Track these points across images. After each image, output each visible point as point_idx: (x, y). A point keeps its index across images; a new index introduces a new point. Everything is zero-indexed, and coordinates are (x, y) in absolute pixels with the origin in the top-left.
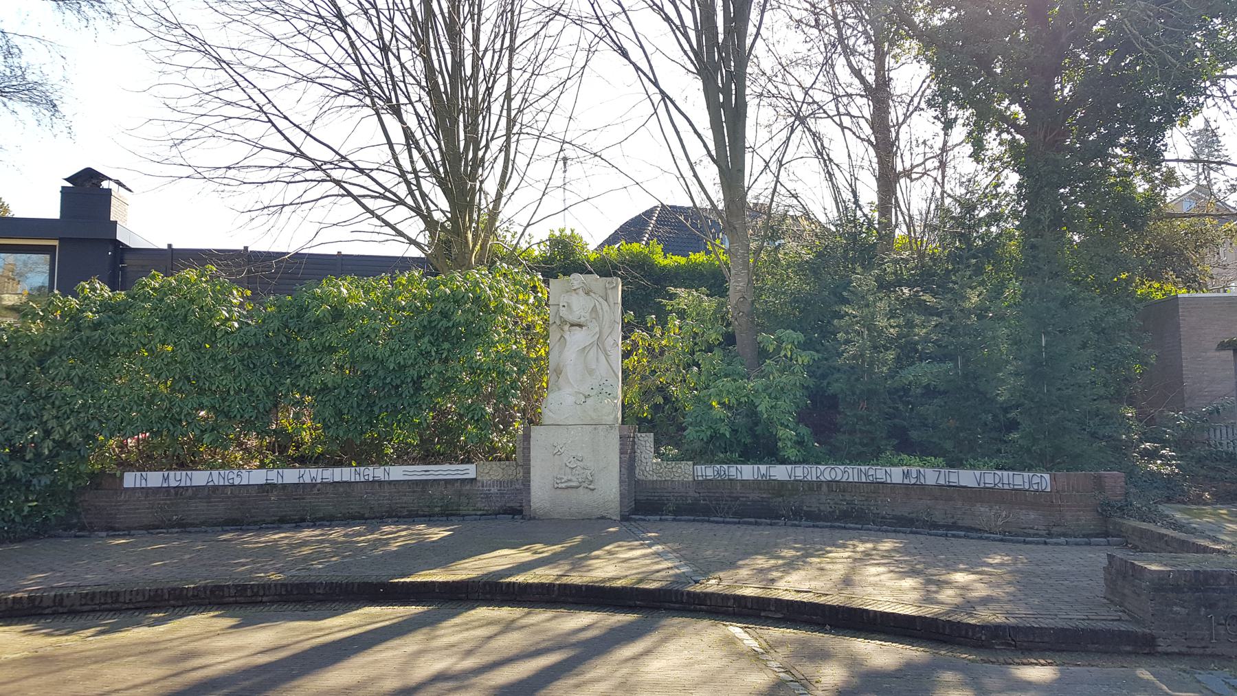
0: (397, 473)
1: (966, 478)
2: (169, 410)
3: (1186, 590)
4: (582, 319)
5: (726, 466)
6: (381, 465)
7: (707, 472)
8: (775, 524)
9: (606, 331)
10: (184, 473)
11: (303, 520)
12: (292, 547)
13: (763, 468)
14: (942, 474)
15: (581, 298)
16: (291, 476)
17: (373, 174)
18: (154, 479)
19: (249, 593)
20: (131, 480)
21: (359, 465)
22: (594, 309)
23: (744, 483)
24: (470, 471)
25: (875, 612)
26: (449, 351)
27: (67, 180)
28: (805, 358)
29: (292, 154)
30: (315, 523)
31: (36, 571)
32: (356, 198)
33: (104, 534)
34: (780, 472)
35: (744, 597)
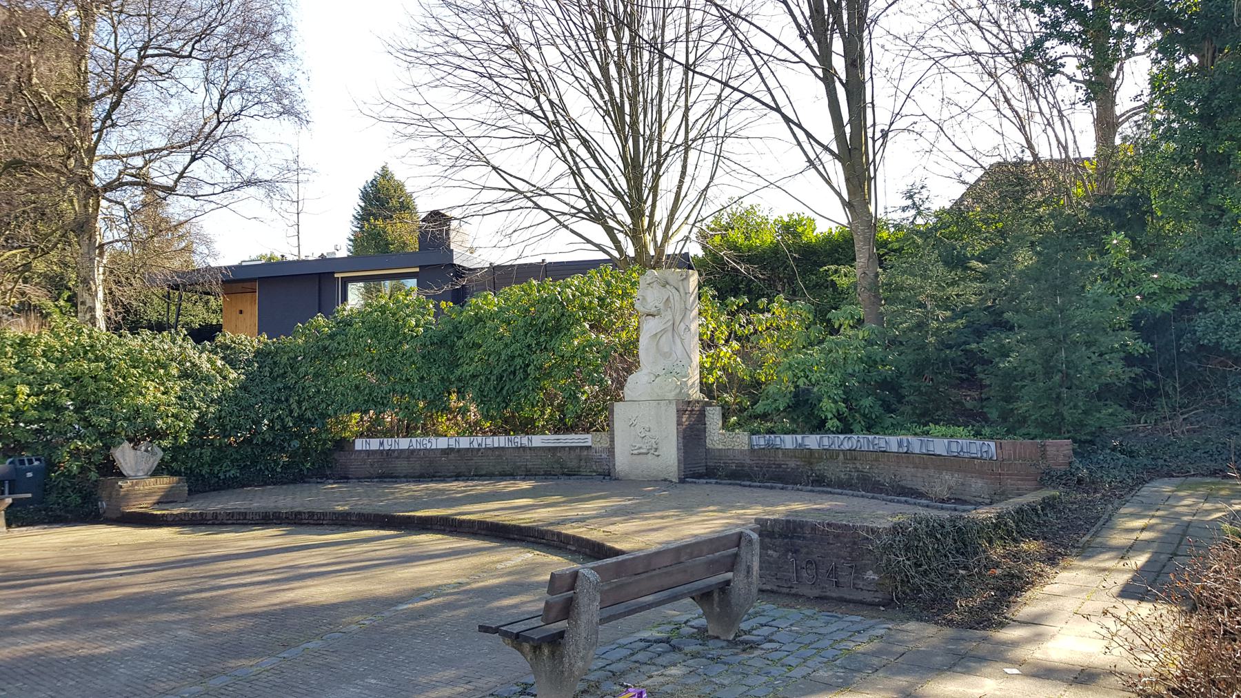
3: (777, 536)
15: (655, 291)
18: (374, 444)
19: (315, 517)
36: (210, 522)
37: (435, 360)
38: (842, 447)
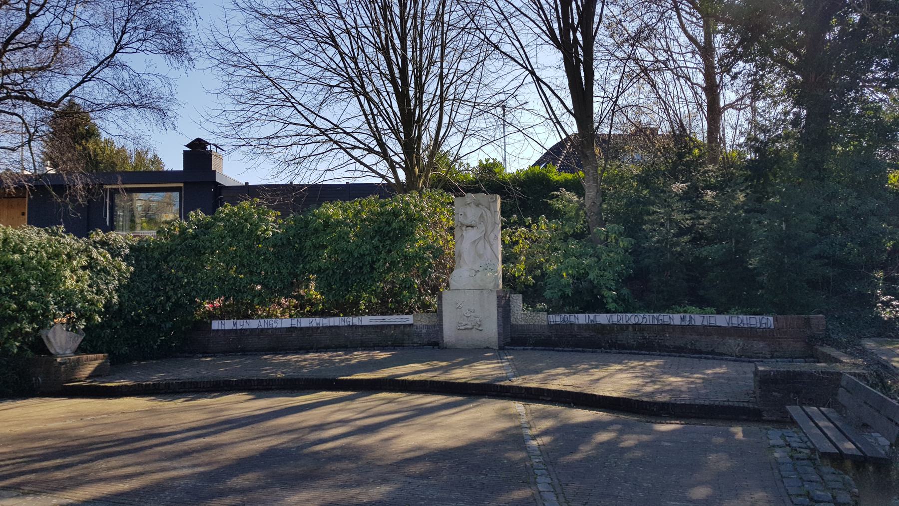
0: (366, 320)
1: (721, 320)
2: (234, 284)
4: (473, 222)
5: (568, 315)
6: (357, 316)
7: (556, 319)
8: (596, 352)
9: (489, 229)
10: (245, 321)
11: (312, 348)
12: (297, 361)
13: (592, 316)
14: (705, 319)
16: (305, 322)
17: (355, 135)
18: (228, 324)
19: (265, 384)
20: (216, 325)
21: (345, 316)
22: (482, 216)
23: (580, 326)
24: (410, 319)
25: (599, 396)
26: (390, 245)
27: (186, 146)
28: (624, 243)
29: (307, 126)
30: (317, 350)
31: (160, 372)
32: (345, 150)
33: (201, 355)
34: (603, 319)
35: (530, 388)
36: (163, 391)
37: (282, 257)
38: (629, 322)
